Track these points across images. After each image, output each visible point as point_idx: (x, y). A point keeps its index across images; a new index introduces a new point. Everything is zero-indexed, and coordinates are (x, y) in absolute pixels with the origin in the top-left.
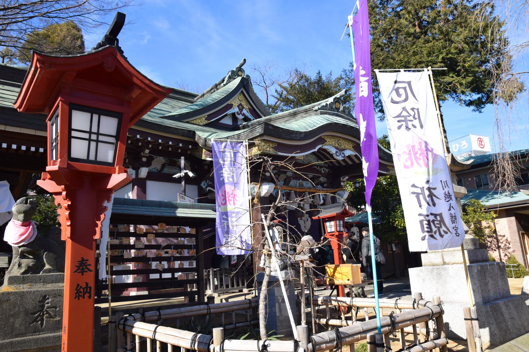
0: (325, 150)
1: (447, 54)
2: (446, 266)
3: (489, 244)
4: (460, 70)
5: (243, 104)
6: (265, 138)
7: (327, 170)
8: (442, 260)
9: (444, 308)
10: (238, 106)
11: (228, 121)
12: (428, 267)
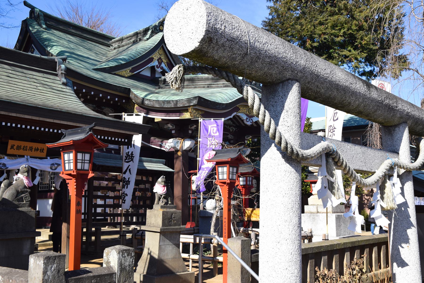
0: (238, 116)
1: (348, 30)
2: (318, 214)
3: (366, 201)
4: (357, 45)
5: (162, 58)
6: (197, 107)
7: (234, 129)
8: (316, 210)
9: (313, 234)
10: (158, 60)
11: (147, 73)
12: (308, 214)
